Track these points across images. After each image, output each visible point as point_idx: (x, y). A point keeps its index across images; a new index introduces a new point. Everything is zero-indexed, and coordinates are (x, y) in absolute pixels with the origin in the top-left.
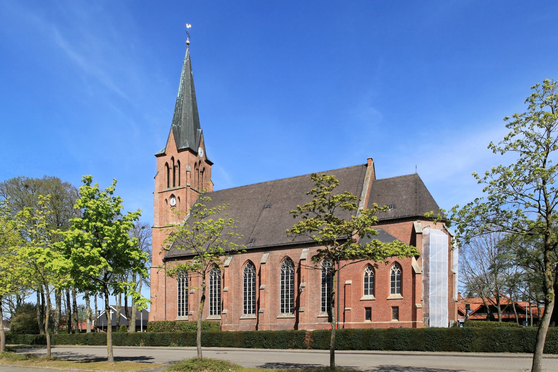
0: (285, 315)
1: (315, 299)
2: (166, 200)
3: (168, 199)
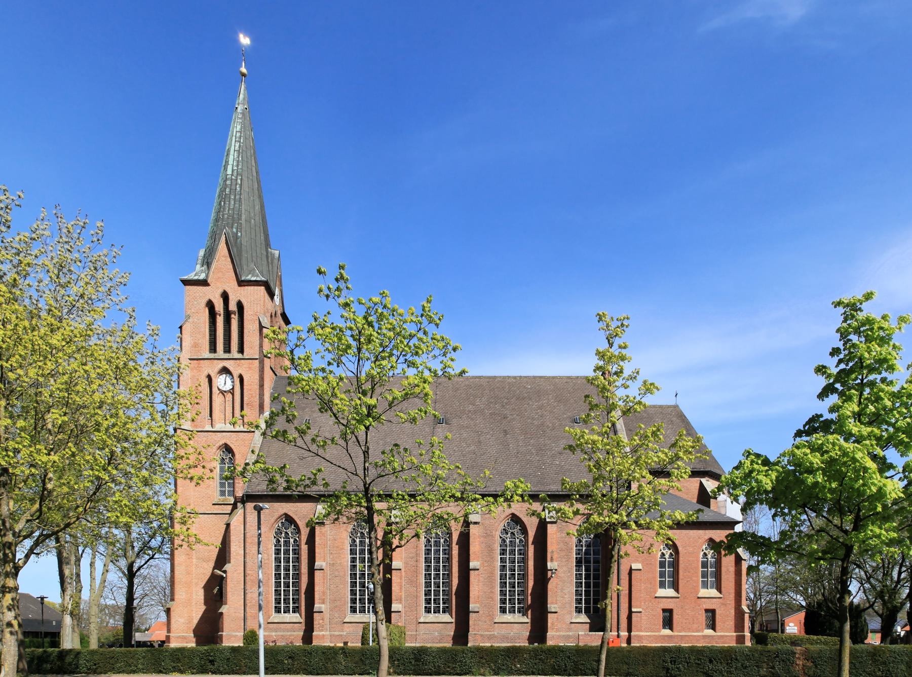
0: (508, 617)
1: (566, 591)
2: (209, 378)
3: (212, 375)
